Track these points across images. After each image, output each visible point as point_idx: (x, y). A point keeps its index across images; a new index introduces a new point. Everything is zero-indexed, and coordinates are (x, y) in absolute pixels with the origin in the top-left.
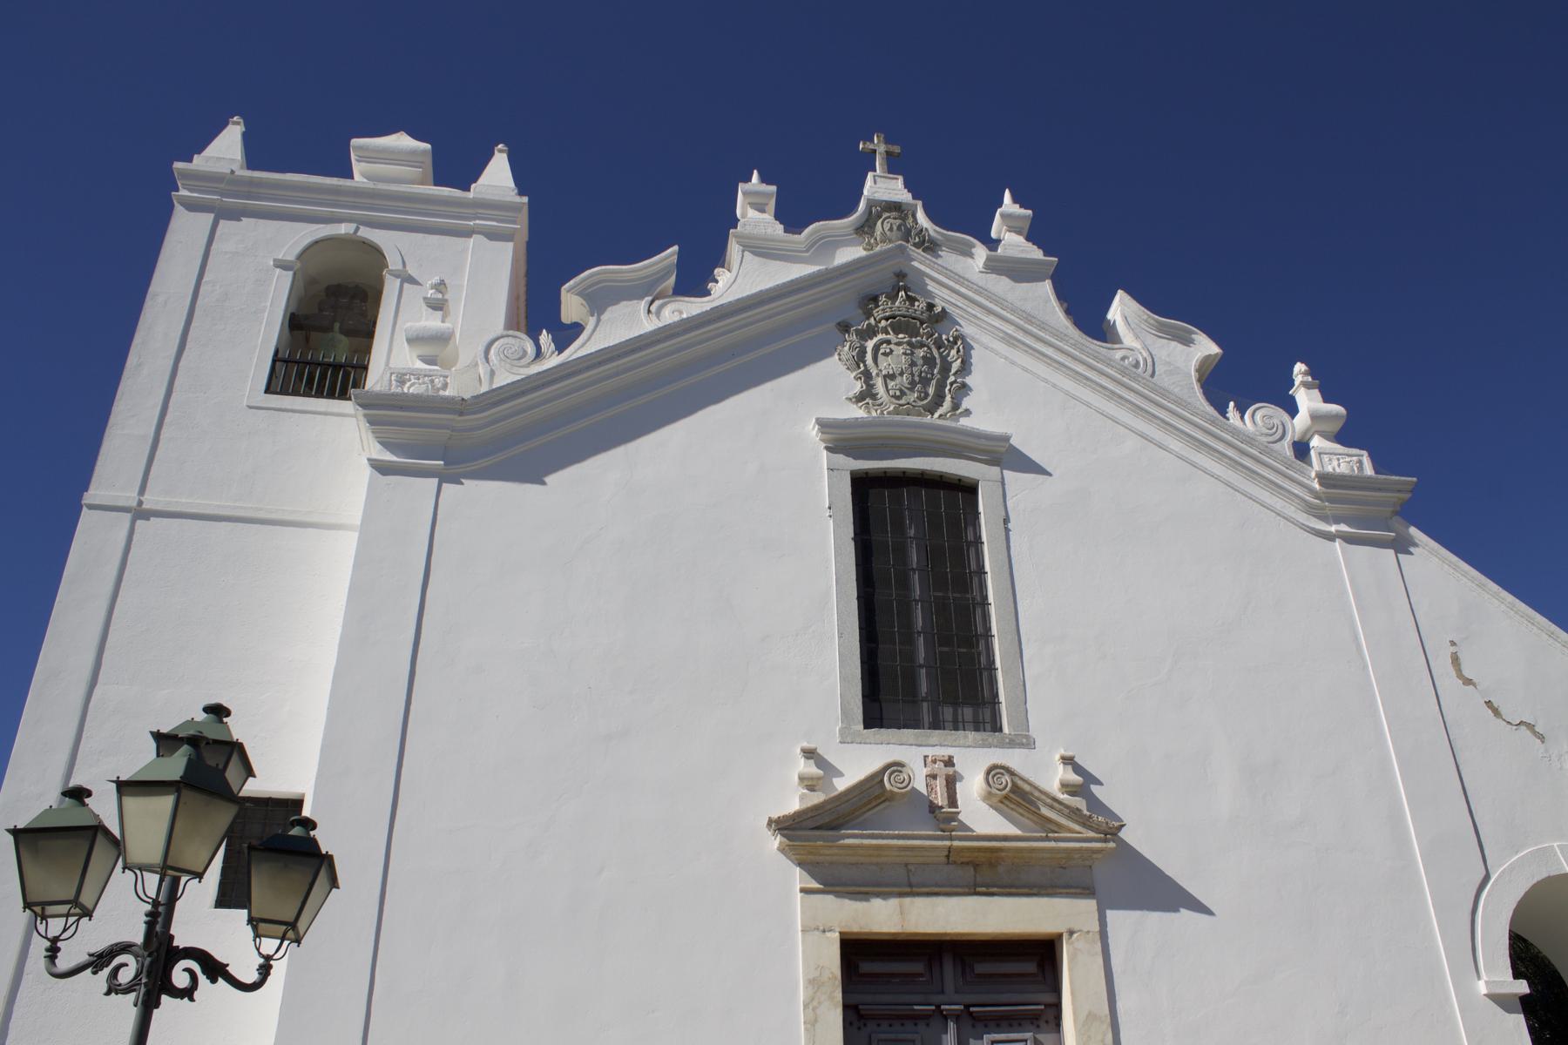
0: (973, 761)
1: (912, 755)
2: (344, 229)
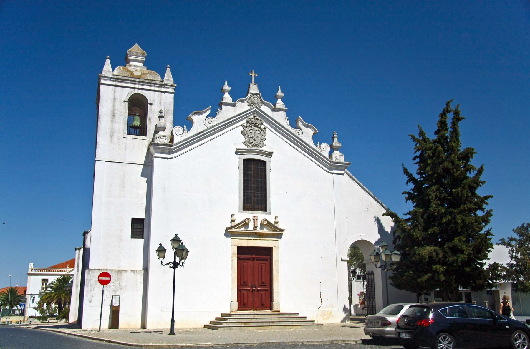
0: (261, 216)
1: (249, 214)
2: (137, 92)
